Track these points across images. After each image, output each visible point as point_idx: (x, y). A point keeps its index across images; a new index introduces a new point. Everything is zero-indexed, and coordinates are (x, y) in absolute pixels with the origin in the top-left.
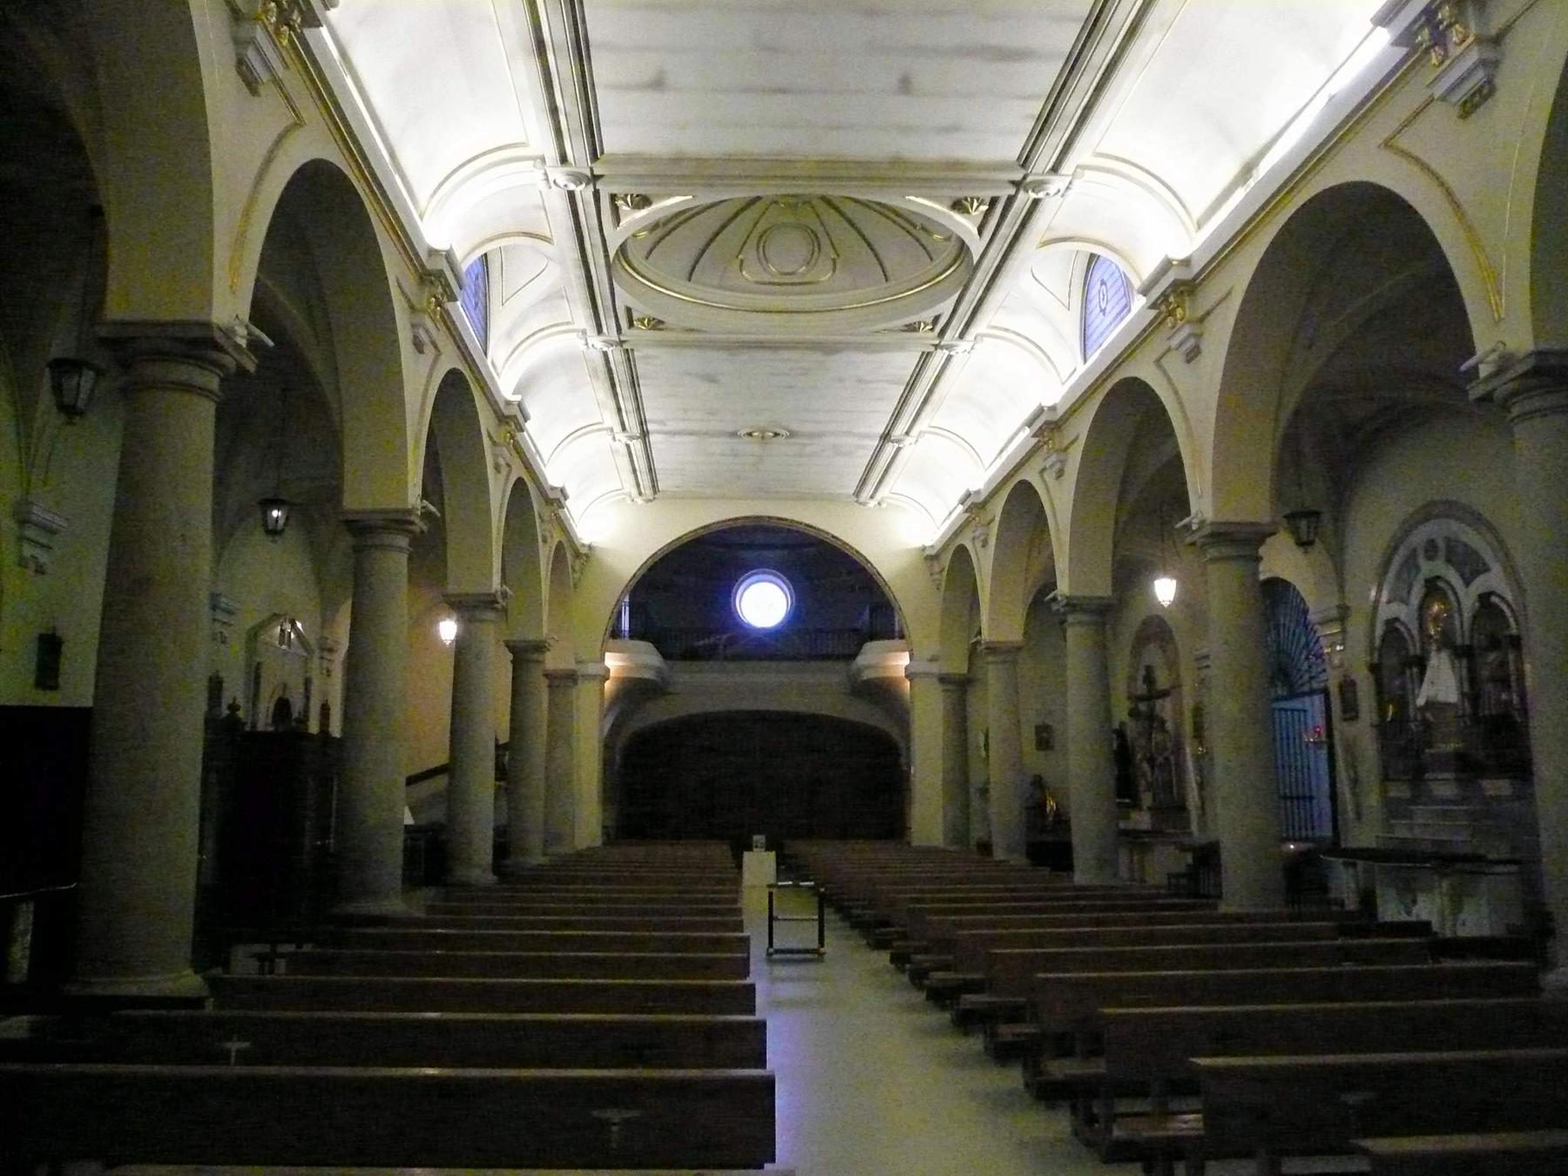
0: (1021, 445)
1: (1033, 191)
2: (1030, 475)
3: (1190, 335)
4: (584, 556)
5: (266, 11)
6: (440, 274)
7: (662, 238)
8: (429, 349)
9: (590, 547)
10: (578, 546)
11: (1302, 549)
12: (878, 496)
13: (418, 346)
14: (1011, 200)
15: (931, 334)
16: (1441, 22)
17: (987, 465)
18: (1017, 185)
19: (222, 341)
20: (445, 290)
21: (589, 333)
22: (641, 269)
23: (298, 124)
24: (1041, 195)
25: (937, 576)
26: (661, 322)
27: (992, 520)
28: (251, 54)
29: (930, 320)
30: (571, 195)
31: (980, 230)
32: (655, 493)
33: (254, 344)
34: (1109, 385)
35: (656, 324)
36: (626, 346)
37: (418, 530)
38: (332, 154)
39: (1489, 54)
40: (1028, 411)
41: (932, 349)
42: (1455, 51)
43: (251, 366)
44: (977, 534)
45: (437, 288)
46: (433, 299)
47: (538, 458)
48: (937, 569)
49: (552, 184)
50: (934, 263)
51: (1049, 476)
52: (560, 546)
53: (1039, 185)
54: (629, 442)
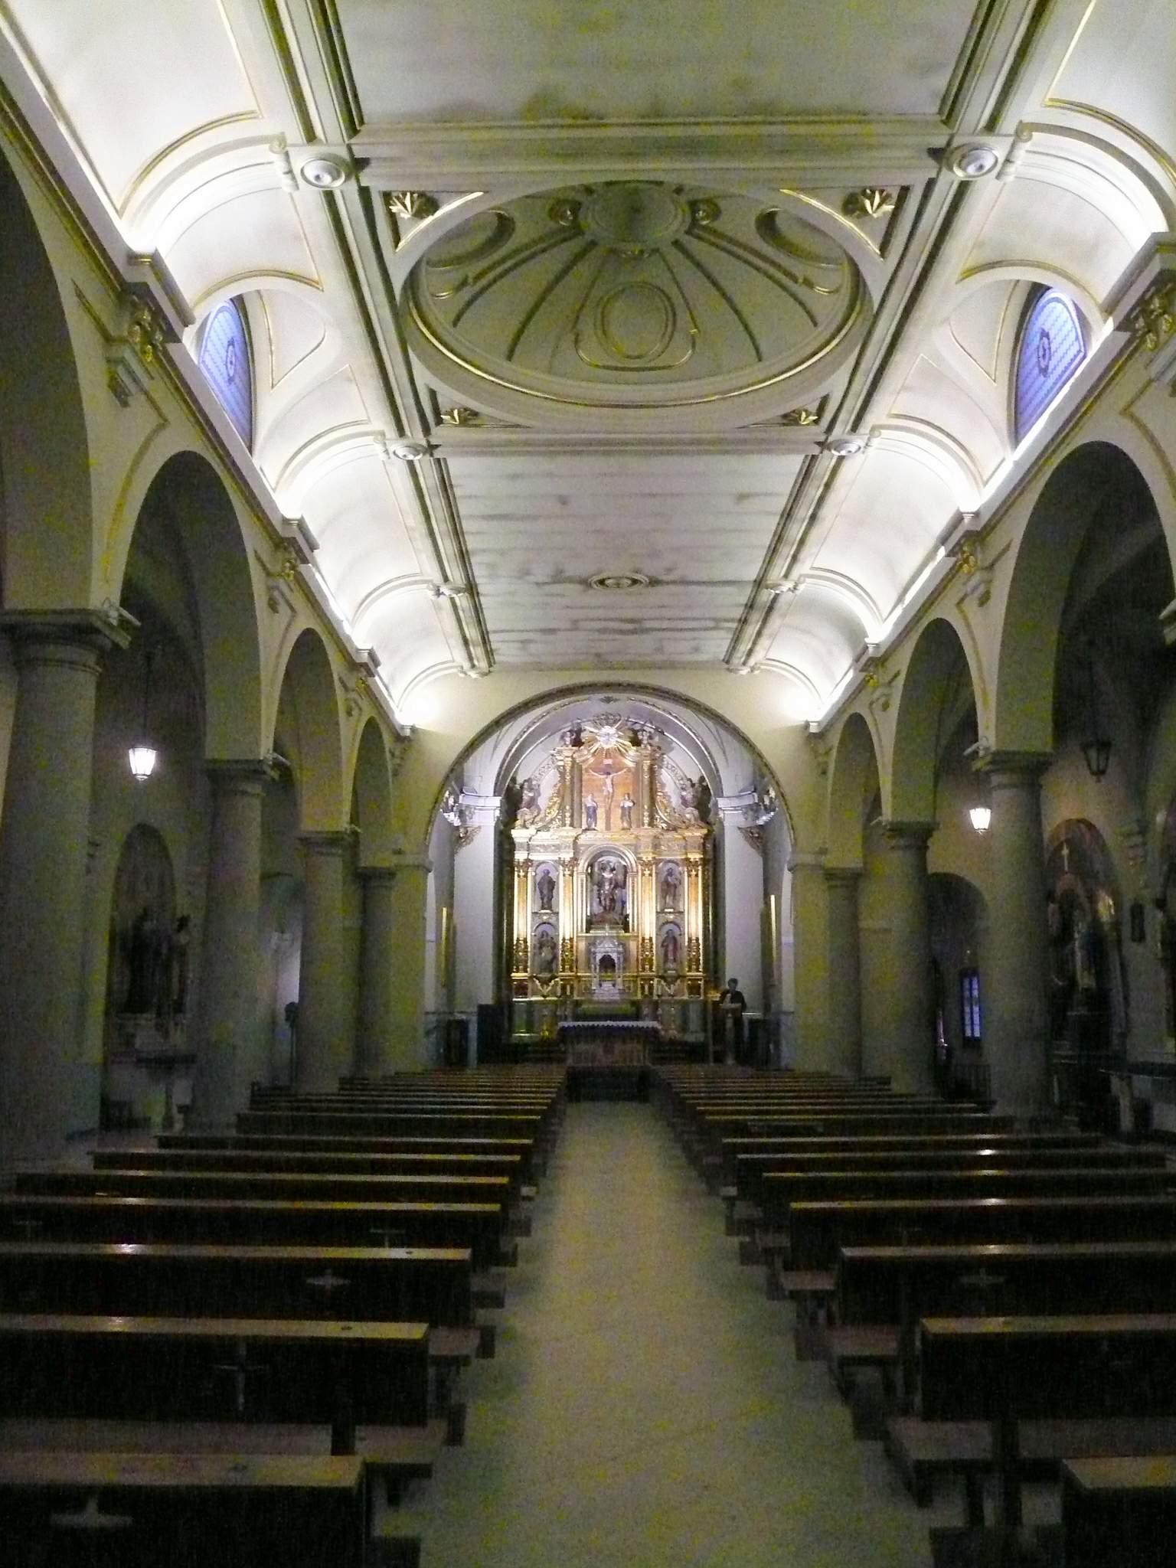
0: (1037, 440)
1: (960, 166)
2: (945, 610)
3: (982, 582)
4: (407, 741)
5: (131, 333)
6: (293, 541)
7: (469, 303)
9: (413, 729)
10: (397, 727)
11: (1094, 778)
12: (752, 662)
13: (273, 606)
14: (930, 184)
15: (814, 429)
16: (1152, 311)
17: (885, 615)
18: (938, 154)
19: (98, 624)
21: (388, 436)
22: (447, 338)
23: (163, 424)
24: (843, 453)
26: (476, 414)
28: (120, 370)
29: (814, 407)
30: (411, 464)
31: (884, 247)
32: (490, 666)
33: (123, 621)
34: (925, 623)
35: (469, 418)
36: (438, 454)
37: (269, 779)
38: (195, 444)
39: (985, 575)
40: (940, 523)
41: (816, 450)
42: (1163, 337)
45: (290, 552)
46: (137, 327)
47: (62, 128)
48: (822, 751)
49: (392, 455)
50: (820, 329)
52: (371, 725)
53: (839, 445)
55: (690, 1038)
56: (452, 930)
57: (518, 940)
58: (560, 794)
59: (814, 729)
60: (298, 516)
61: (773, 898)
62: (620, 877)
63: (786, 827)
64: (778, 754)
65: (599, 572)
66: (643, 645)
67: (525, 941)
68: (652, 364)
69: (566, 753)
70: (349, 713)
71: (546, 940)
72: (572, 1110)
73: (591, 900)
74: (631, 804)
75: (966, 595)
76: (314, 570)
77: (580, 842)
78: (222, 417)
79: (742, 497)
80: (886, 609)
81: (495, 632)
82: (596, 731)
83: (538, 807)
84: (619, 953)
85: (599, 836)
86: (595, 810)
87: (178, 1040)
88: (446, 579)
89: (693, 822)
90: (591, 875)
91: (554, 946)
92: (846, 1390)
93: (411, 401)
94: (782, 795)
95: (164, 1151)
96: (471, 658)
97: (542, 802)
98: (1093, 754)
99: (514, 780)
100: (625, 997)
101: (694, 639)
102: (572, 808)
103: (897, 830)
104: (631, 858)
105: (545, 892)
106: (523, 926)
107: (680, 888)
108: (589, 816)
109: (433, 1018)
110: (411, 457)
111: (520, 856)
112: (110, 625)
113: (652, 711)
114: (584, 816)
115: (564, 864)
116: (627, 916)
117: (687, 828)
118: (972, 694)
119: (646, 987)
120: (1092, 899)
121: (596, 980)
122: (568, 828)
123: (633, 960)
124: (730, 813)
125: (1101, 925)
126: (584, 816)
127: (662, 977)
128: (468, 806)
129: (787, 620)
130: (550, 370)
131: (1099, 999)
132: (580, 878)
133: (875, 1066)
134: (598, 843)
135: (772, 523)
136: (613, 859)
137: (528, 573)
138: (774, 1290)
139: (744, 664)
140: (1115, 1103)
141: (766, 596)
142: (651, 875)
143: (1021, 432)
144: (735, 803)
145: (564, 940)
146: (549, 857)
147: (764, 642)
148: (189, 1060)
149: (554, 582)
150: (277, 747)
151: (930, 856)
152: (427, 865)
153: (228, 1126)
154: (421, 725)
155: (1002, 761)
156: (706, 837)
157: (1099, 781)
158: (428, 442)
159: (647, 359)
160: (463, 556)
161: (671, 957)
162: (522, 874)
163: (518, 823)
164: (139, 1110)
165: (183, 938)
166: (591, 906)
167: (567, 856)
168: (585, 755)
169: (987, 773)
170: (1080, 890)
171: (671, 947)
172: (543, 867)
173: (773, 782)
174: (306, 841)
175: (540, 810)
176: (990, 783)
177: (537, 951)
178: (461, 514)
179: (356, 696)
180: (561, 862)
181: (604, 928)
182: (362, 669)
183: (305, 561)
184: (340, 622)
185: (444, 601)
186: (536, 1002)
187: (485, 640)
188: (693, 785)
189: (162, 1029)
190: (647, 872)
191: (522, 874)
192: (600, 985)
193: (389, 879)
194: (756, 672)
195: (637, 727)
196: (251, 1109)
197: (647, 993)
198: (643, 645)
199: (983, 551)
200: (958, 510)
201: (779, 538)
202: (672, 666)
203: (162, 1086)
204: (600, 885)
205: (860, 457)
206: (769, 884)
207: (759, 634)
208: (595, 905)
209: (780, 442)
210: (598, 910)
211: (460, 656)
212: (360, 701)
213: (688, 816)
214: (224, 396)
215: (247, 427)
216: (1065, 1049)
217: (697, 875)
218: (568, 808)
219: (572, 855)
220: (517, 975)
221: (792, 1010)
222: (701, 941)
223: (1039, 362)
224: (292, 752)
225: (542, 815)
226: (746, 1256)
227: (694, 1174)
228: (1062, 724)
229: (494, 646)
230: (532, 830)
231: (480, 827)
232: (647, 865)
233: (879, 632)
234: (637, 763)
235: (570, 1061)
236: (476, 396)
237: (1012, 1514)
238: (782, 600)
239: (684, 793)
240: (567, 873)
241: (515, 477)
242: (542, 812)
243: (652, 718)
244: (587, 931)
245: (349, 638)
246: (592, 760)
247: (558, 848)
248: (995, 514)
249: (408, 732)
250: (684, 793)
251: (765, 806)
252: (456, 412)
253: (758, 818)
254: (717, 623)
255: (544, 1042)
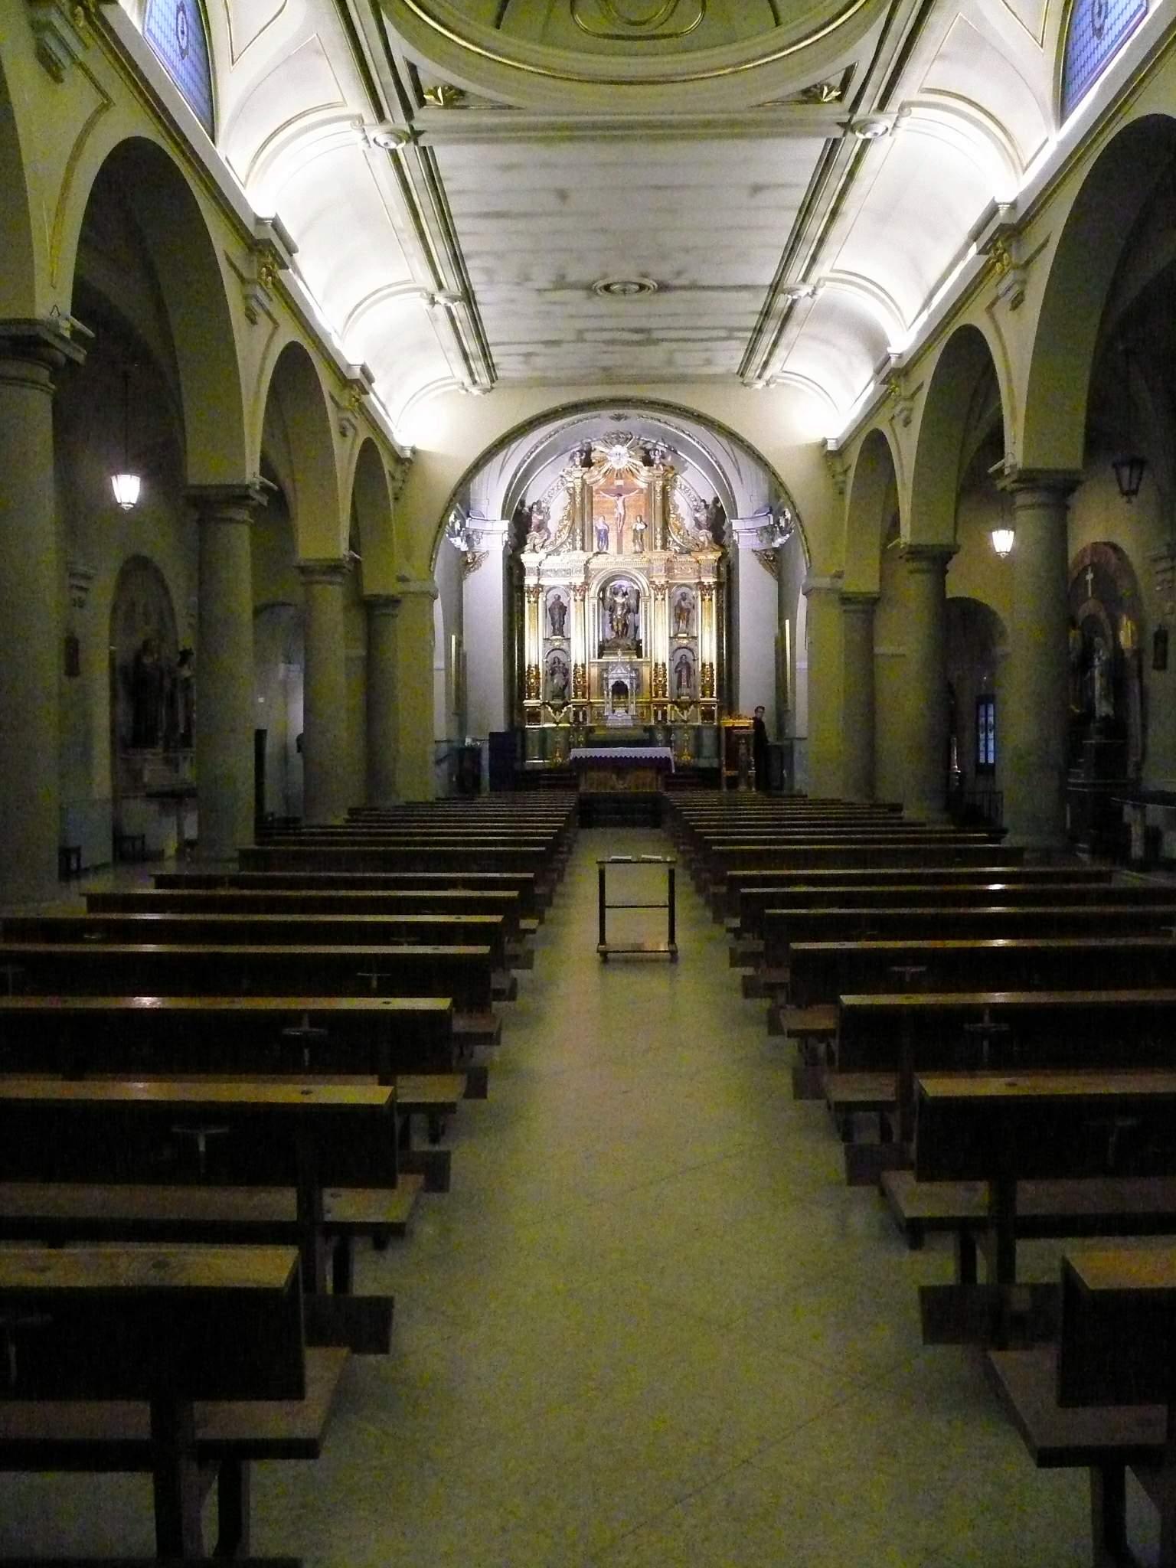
1: (860, 131)
2: (975, 316)
3: (1015, 282)
4: (408, 463)
8: (262, 319)
9: (414, 451)
11: (1125, 499)
12: (767, 375)
15: (837, 105)
19: (50, 338)
20: (274, 259)
21: (366, 121)
23: (106, 105)
24: (869, 135)
25: (841, 478)
26: (461, 93)
27: (919, 388)
29: (836, 81)
30: (394, 154)
32: (492, 381)
33: (75, 333)
34: (950, 331)
39: (1020, 275)
40: (972, 217)
41: (838, 133)
43: (80, 357)
44: (1003, 286)
46: (264, 269)
48: (839, 469)
49: (372, 143)
51: (898, 425)
52: (368, 448)
53: (864, 126)
54: (450, 304)
55: (703, 763)
56: (461, 657)
57: (529, 666)
58: (570, 517)
59: (831, 446)
60: (273, 216)
61: (787, 622)
62: (633, 602)
63: (801, 550)
64: (795, 473)
65: (605, 276)
66: (652, 357)
67: (537, 667)
68: (659, 31)
69: (576, 474)
70: (343, 434)
71: (558, 667)
72: (583, 834)
73: (604, 624)
74: (643, 527)
75: (997, 298)
76: (295, 277)
77: (591, 566)
78: (172, 92)
79: (757, 189)
80: (910, 315)
81: (497, 344)
82: (606, 450)
83: (547, 530)
84: (631, 678)
85: (611, 559)
86: (606, 533)
87: (188, 773)
88: (440, 286)
89: (706, 544)
90: (603, 599)
91: (566, 672)
92: (846, 1132)
93: (389, 78)
94: (797, 516)
95: (160, 891)
96: (471, 374)
97: (552, 525)
98: (1126, 472)
99: (522, 503)
100: (639, 723)
101: (707, 350)
102: (583, 532)
103: (915, 553)
104: (644, 581)
105: (557, 617)
106: (535, 652)
107: (693, 612)
108: (599, 539)
109: (444, 747)
110: (393, 145)
111: (530, 581)
112: (62, 338)
113: (666, 430)
114: (595, 540)
115: (575, 589)
116: (640, 641)
117: (701, 551)
118: (1000, 409)
119: (660, 712)
120: (1116, 628)
121: (610, 706)
122: (579, 551)
123: (646, 688)
124: (745, 534)
125: (1122, 652)
126: (595, 540)
127: (675, 703)
128: (474, 531)
129: (805, 329)
130: (545, 39)
131: (1116, 727)
132: (592, 601)
133: (886, 794)
134: (610, 567)
135: (790, 218)
136: (625, 584)
137: (527, 279)
138: (774, 1026)
139: (759, 377)
140: (1127, 829)
141: (782, 302)
142: (663, 599)
143: (1069, 106)
144: (750, 525)
145: (576, 666)
146: (561, 582)
147: (780, 352)
148: (191, 793)
149: (556, 289)
150: (266, 468)
151: (950, 578)
152: (432, 591)
153: (231, 860)
154: (420, 446)
155: (1028, 479)
156: (720, 559)
157: (1129, 502)
158: (412, 128)
159: (652, 25)
160: (458, 260)
161: (684, 683)
162: (532, 599)
163: (528, 547)
164: (152, 844)
165: (186, 672)
166: (604, 631)
167: (578, 580)
168: (595, 475)
169: (1012, 492)
170: (1103, 615)
171: (684, 673)
172: (553, 593)
173: (789, 503)
174: (303, 570)
175: (549, 533)
176: (1014, 503)
177: (549, 677)
178: (452, 213)
179: (349, 415)
180: (572, 587)
181: (616, 654)
182: (355, 386)
183: (284, 266)
184: (328, 335)
185: (440, 311)
186: (549, 728)
187: (486, 354)
188: (706, 506)
189: (172, 764)
190: (660, 597)
191: (532, 599)
192: (614, 712)
193: (394, 608)
194: (772, 386)
195: (649, 446)
196: (257, 844)
197: (660, 719)
198: (652, 357)
199: (1018, 248)
200: (993, 200)
201: (797, 236)
202: (682, 379)
203: (173, 819)
204: (612, 610)
205: (887, 139)
206: (784, 609)
207: (775, 344)
208: (608, 630)
209: (801, 123)
210: (610, 635)
211: (460, 372)
212: (353, 420)
213: (702, 539)
214: (177, 72)
215: (208, 114)
216: (1081, 778)
217: (711, 600)
218: (578, 531)
219: (583, 580)
220: (528, 702)
221: (805, 736)
222: (715, 667)
223: (1093, 21)
224: (282, 473)
225: (552, 538)
226: (749, 989)
227: (701, 901)
228: (1095, 442)
229: (495, 360)
230: (542, 554)
231: (488, 552)
232: (660, 589)
233: (902, 341)
234: (650, 484)
235: (582, 789)
236: (458, 71)
237: (1005, 1267)
238: (799, 308)
239: (697, 515)
240: (579, 598)
241: (508, 168)
242: (552, 536)
243: (664, 436)
244: (600, 656)
245: (339, 353)
246: (602, 481)
247: (568, 572)
248: (1034, 204)
249: (408, 454)
250: (697, 515)
251: (781, 528)
252: (439, 91)
253: (773, 540)
254: (731, 333)
255: (560, 769)
